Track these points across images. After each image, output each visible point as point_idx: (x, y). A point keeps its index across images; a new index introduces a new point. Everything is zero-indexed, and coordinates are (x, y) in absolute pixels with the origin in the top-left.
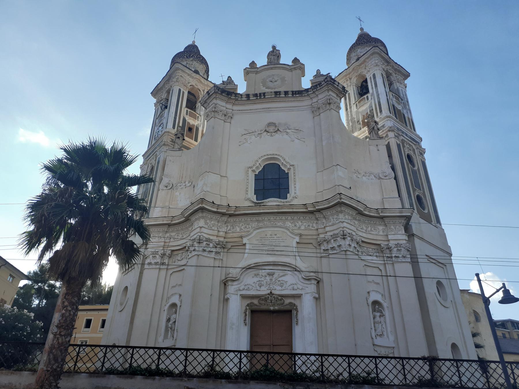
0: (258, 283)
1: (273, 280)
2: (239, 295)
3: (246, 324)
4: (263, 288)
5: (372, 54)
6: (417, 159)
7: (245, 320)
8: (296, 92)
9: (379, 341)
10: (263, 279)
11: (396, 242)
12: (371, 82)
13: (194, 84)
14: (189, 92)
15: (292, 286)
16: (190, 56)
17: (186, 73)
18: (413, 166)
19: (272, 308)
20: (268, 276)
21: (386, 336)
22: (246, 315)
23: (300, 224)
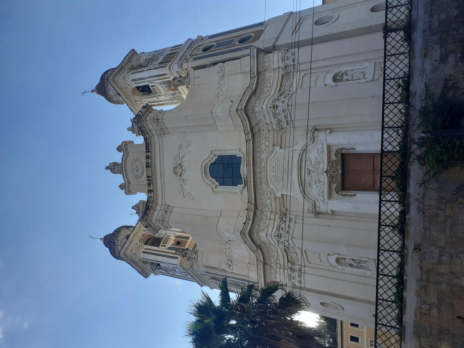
0: (317, 184)
1: (314, 170)
2: (328, 201)
3: (355, 195)
4: (322, 179)
5: (115, 82)
6: (207, 43)
7: (351, 196)
8: (146, 149)
9: (369, 76)
10: (314, 179)
11: (280, 61)
12: (139, 83)
13: (139, 239)
14: (146, 244)
15: (320, 153)
16: (113, 243)
17: (128, 246)
18: (212, 46)
19: (340, 171)
20: (311, 175)
21: (365, 70)
22: (346, 195)
23: (263, 145)
